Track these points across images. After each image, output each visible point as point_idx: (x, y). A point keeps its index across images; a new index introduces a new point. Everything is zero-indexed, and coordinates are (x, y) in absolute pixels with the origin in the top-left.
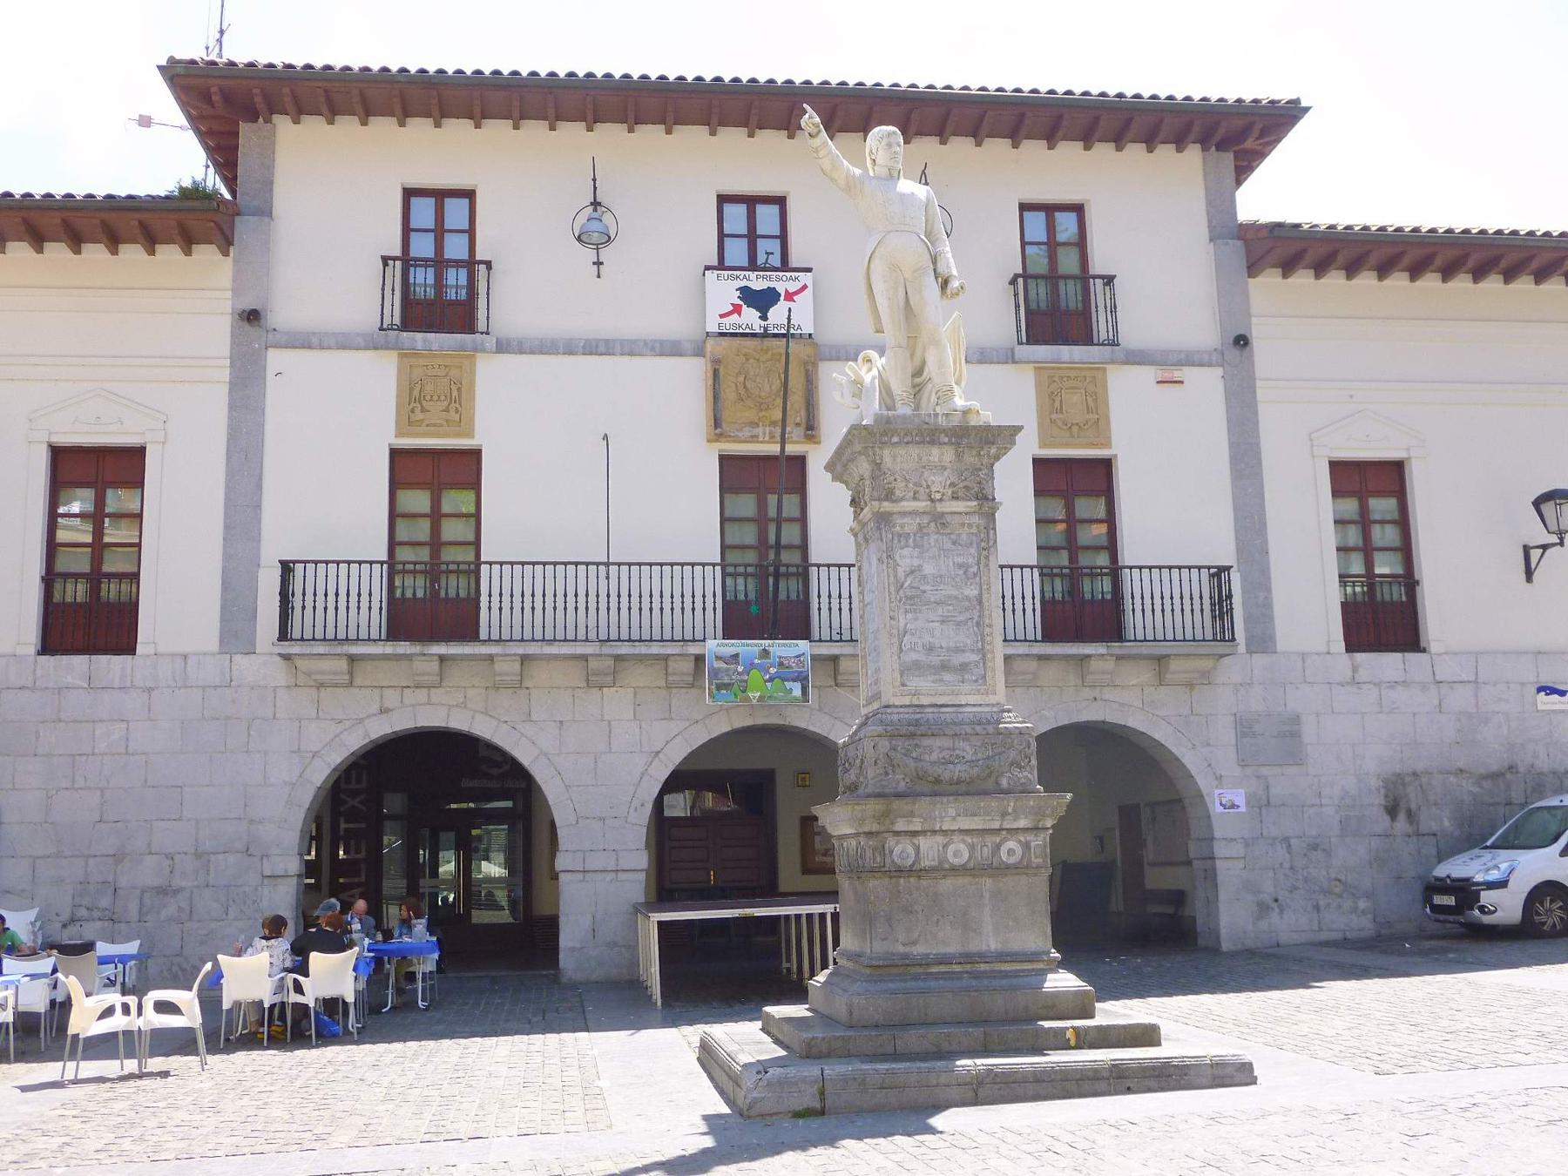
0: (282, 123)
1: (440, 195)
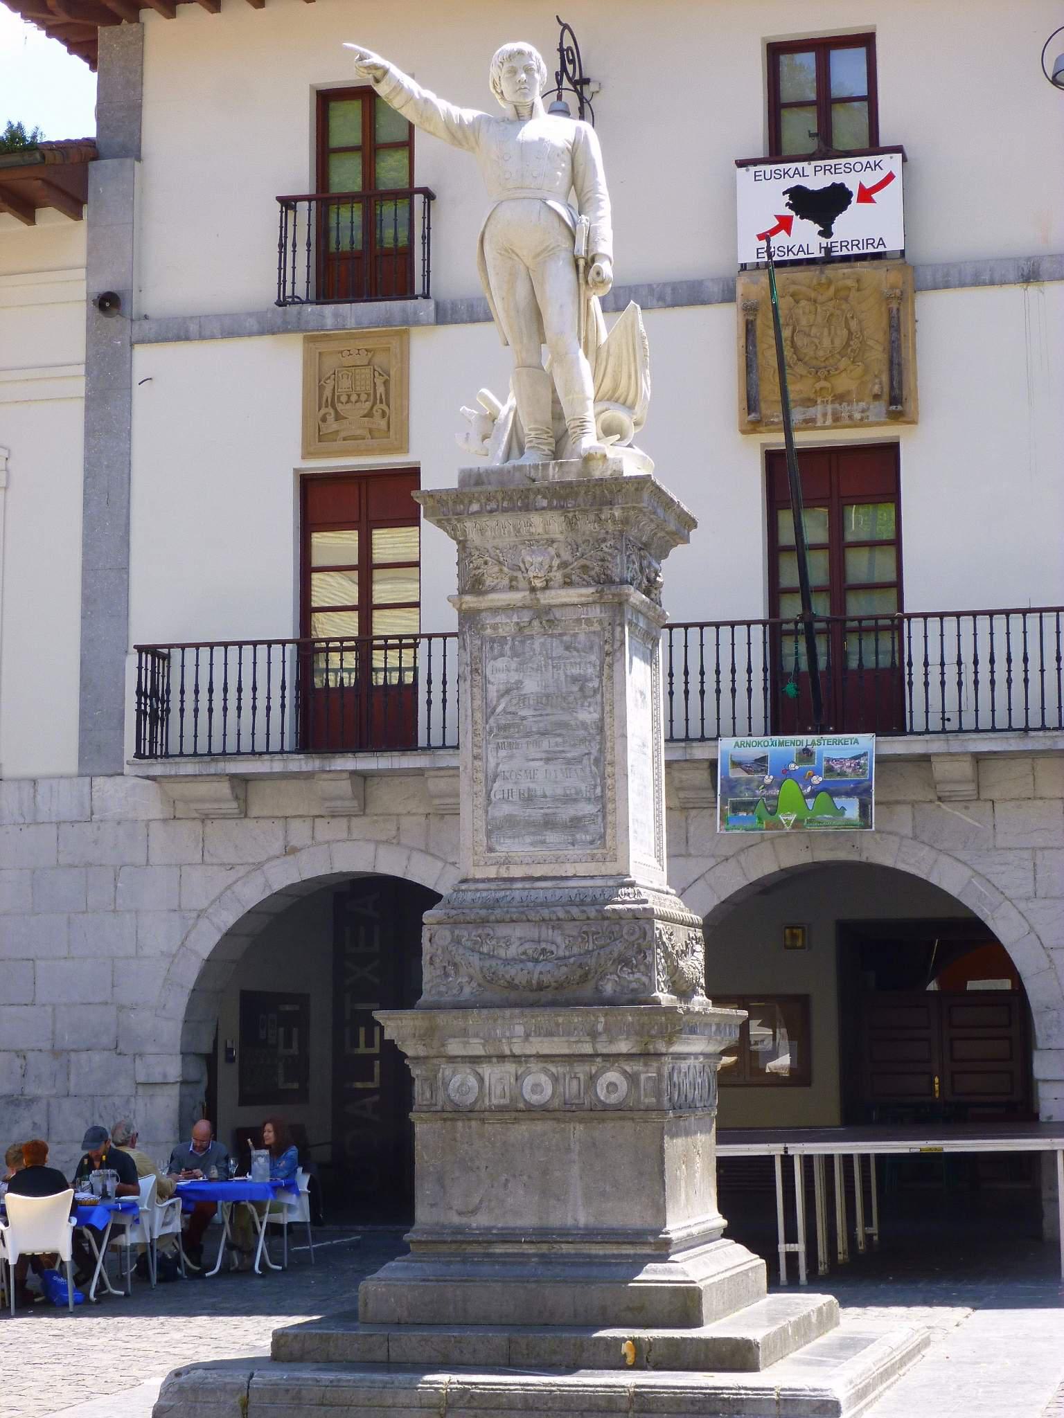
0: (152, 20)
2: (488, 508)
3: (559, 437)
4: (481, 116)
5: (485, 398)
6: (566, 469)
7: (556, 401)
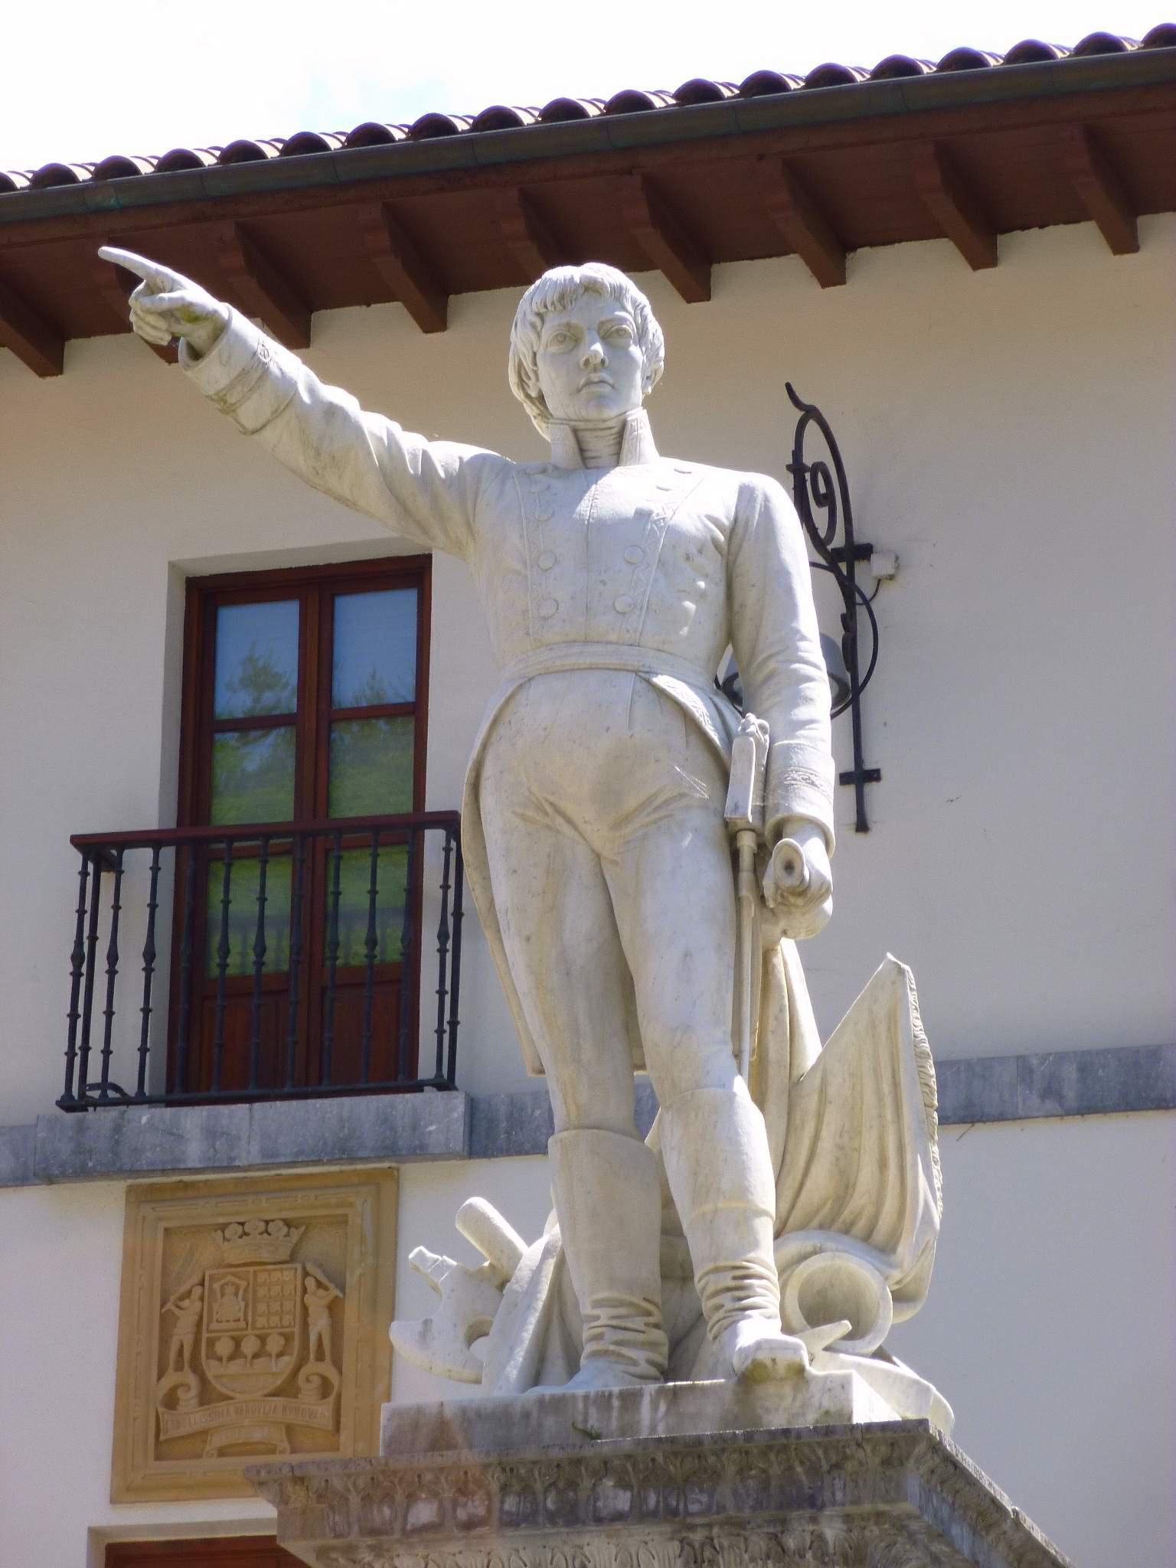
1: (317, 590)
2: (462, 1514)
3: (678, 1315)
4: (483, 458)
5: (479, 1221)
6: (688, 1406)
7: (671, 1231)
